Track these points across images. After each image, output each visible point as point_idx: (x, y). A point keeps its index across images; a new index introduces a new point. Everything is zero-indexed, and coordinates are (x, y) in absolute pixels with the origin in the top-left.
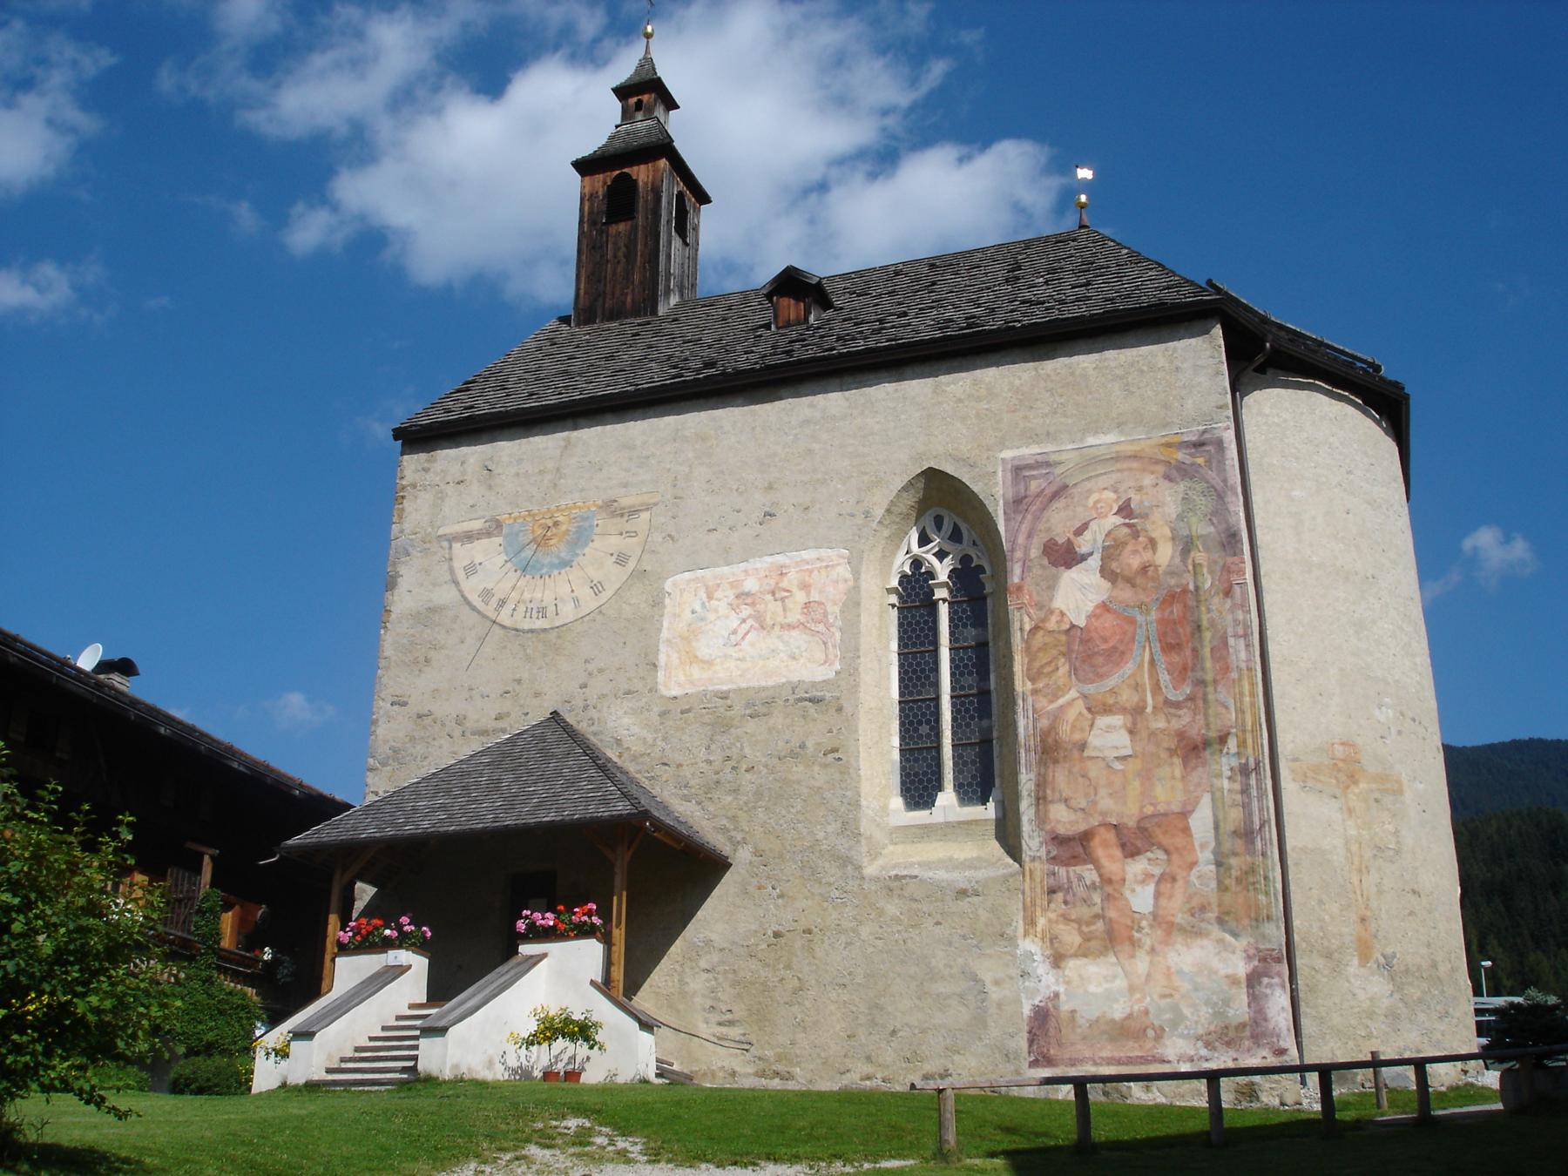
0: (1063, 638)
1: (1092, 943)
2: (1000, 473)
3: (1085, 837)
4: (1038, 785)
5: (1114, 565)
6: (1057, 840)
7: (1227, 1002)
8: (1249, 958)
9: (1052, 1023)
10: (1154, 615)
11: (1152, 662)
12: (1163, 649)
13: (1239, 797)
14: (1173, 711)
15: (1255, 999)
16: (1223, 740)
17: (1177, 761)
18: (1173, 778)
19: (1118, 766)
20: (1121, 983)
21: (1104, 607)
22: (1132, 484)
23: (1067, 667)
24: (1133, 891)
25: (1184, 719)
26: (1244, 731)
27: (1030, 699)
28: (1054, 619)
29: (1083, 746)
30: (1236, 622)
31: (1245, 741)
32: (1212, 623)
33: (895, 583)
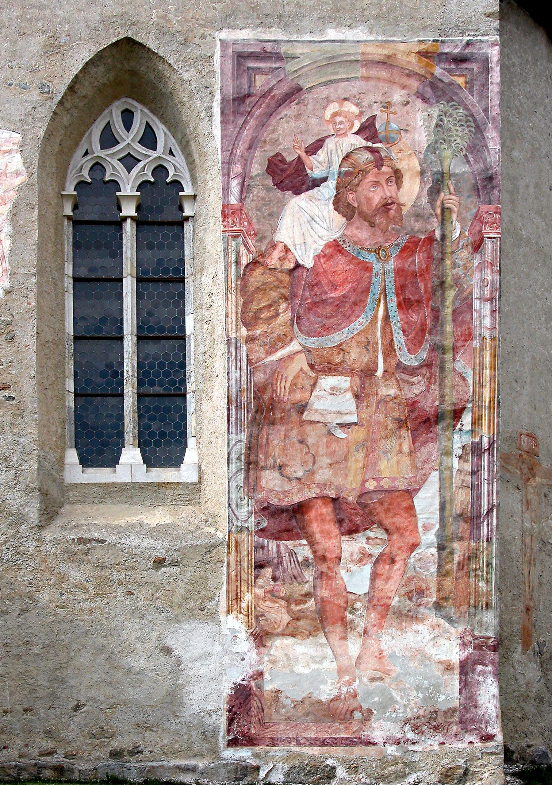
0: (286, 278)
1: (302, 623)
2: (217, 60)
3: (300, 509)
4: (249, 448)
5: (351, 197)
7: (437, 687)
8: (464, 645)
9: (255, 703)
10: (391, 265)
11: (387, 318)
12: (399, 305)
13: (468, 478)
14: (406, 377)
15: (466, 685)
16: (457, 414)
17: (406, 434)
18: (400, 452)
19: (340, 434)
20: (329, 665)
21: (336, 247)
22: (379, 98)
23: (289, 314)
25: (416, 388)
26: (480, 407)
27: (244, 348)
28: (276, 254)
29: (302, 408)
31: (480, 418)
32: (457, 282)
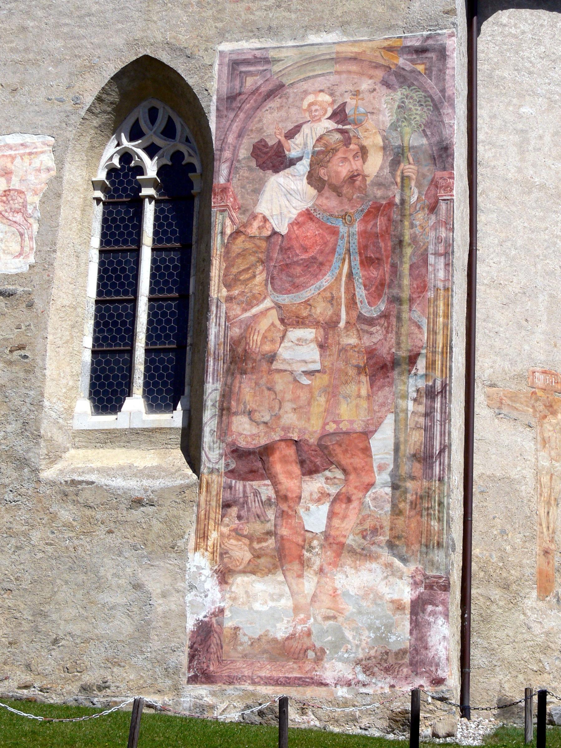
3: (266, 452)
4: (223, 396)
6: (238, 453)
9: (214, 640)
11: (350, 275)
12: (362, 263)
16: (412, 360)
18: (359, 396)
24: (308, 509)
26: (434, 352)
27: (224, 307)
28: (256, 224)
29: (272, 358)
30: (438, 240)
33: (102, 175)
